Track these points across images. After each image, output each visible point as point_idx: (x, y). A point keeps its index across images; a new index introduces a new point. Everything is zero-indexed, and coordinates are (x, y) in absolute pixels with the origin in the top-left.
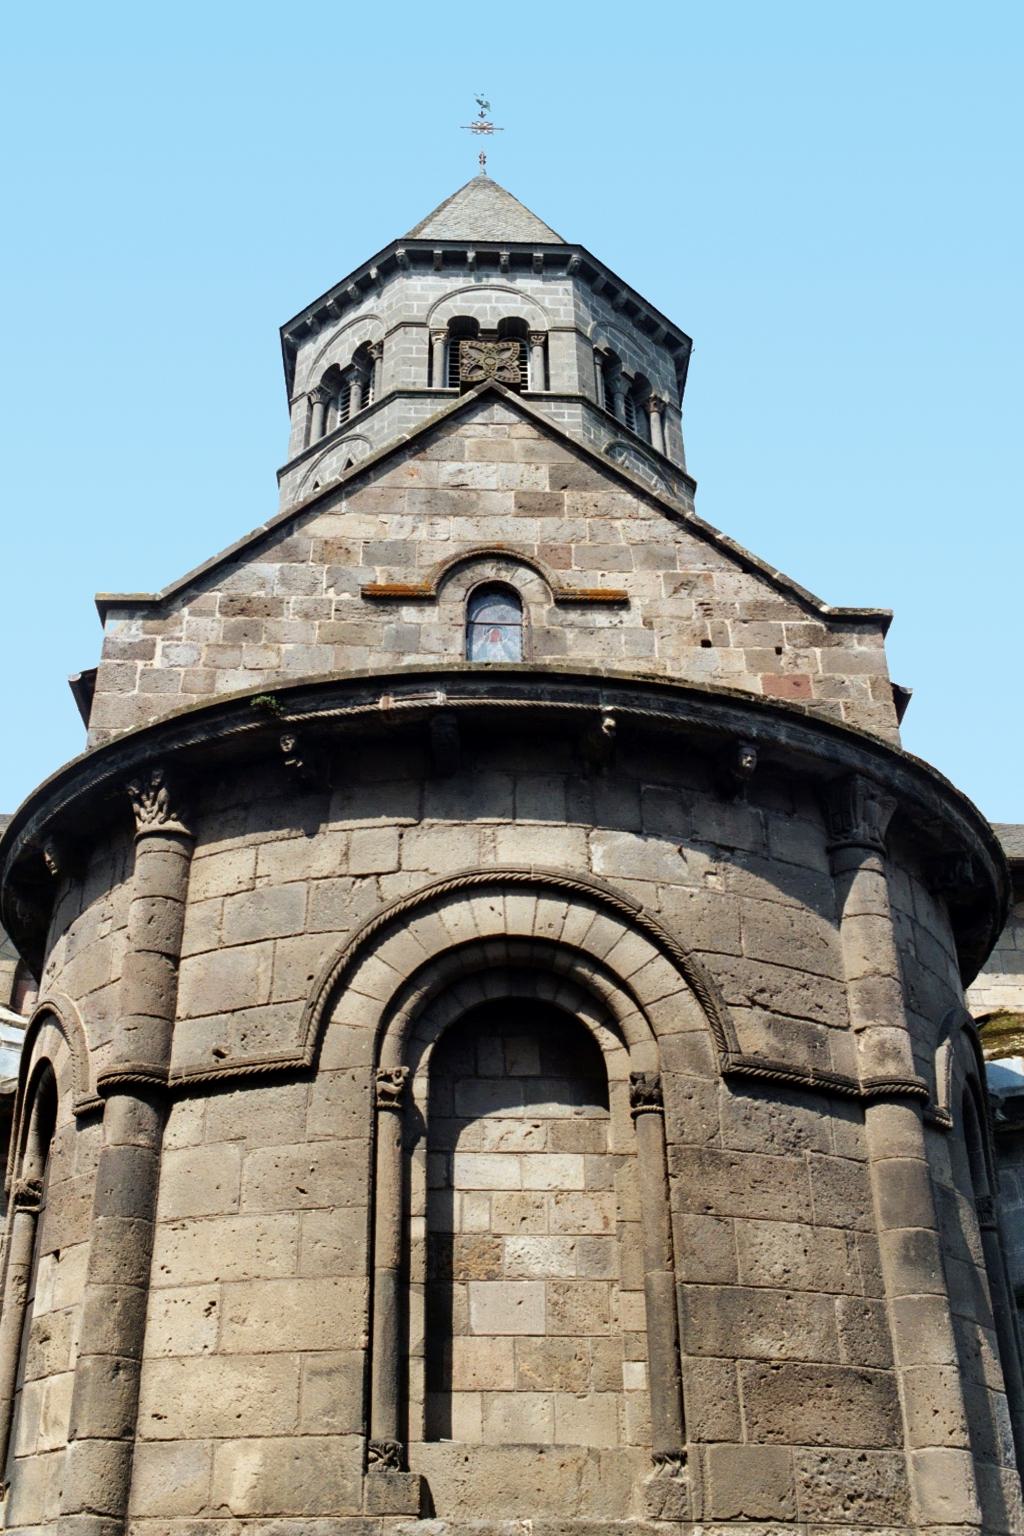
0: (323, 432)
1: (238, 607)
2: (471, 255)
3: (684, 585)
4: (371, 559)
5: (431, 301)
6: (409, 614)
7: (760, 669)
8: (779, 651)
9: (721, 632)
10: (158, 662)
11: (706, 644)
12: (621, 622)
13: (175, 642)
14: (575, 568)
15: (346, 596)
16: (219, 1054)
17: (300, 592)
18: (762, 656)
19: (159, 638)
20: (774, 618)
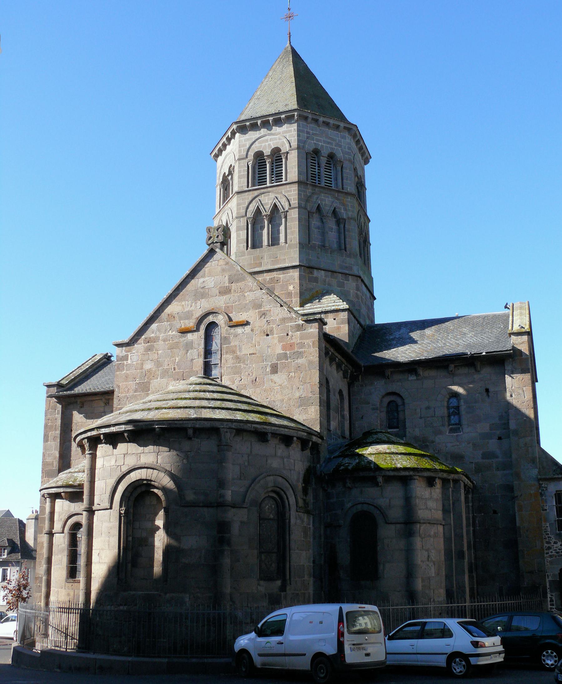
0: (232, 193)
1: (148, 341)
2: (259, 122)
3: (264, 314)
4: (181, 319)
5: (248, 146)
6: (189, 336)
7: (281, 342)
8: (288, 335)
9: (272, 331)
10: (129, 362)
11: (268, 335)
12: (245, 331)
13: (133, 354)
14: (234, 313)
15: (174, 333)
16: (522, 327)
17: (162, 333)
18: (283, 337)
19: (129, 353)
20: (287, 323)
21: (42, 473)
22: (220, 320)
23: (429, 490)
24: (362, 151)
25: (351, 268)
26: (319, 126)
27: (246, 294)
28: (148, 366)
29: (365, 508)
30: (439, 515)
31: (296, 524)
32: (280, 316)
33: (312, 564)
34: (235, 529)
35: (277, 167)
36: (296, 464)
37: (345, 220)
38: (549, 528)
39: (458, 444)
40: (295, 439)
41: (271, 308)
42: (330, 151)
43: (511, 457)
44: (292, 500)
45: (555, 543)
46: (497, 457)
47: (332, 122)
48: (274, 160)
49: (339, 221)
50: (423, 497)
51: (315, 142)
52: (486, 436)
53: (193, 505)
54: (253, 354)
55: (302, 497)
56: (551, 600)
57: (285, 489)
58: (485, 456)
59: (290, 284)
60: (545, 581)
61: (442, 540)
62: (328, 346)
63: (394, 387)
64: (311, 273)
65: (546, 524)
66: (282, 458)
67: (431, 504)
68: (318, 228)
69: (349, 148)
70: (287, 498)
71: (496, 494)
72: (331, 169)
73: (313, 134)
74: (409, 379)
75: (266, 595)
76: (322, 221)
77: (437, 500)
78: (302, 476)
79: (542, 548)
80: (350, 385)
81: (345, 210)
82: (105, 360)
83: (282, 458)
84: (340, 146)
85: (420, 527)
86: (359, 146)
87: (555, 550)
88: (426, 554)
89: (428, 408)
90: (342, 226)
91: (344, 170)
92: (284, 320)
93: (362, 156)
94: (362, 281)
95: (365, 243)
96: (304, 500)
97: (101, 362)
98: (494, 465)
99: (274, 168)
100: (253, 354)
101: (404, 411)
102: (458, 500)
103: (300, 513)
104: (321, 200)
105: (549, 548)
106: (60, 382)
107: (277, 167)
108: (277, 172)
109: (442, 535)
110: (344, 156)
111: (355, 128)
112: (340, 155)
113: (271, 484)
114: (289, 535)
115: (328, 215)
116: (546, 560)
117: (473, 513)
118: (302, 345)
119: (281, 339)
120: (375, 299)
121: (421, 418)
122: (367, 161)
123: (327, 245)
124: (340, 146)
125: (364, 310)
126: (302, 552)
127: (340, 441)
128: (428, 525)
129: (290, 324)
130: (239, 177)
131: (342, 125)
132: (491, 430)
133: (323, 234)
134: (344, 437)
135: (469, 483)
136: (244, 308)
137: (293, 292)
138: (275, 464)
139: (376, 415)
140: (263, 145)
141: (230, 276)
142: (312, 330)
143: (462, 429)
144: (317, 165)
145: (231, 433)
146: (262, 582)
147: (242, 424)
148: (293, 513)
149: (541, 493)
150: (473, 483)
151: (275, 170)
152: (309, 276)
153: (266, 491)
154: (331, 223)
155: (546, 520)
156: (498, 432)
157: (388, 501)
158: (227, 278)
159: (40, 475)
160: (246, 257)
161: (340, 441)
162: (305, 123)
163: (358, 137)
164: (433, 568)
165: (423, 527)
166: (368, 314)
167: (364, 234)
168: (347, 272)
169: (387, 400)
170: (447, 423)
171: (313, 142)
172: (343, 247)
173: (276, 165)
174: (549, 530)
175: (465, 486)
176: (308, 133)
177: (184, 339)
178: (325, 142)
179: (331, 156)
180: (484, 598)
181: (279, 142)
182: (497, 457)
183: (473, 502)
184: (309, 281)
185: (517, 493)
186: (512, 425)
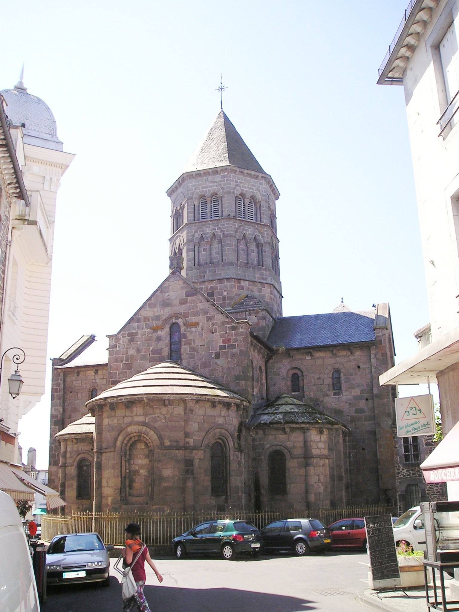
11: (213, 333)
19: (117, 343)
21: (51, 422)
22: (180, 321)
23: (319, 436)
24: (274, 192)
25: (266, 279)
26: (244, 176)
27: (197, 305)
28: (131, 352)
29: (278, 448)
30: (326, 452)
31: (233, 459)
32: (221, 320)
33: (243, 485)
34: (196, 463)
35: (214, 206)
36: (233, 420)
37: (262, 244)
38: (399, 460)
39: (339, 403)
40: (233, 404)
41: (215, 314)
42: (252, 195)
43: (374, 412)
44: (231, 444)
45: (403, 469)
46: (365, 412)
47: (253, 173)
48: (213, 201)
49: (259, 245)
50: (315, 441)
51: (241, 188)
52: (357, 398)
53: (170, 448)
54: (203, 345)
55: (237, 441)
56: (400, 508)
57: (226, 437)
58: (357, 411)
59: (225, 291)
60: (396, 495)
61: (328, 468)
62: (253, 339)
63: (296, 364)
64: (240, 283)
65: (397, 457)
66: (224, 417)
67: (321, 445)
68: (243, 250)
69: (265, 192)
70: (228, 443)
71: (365, 437)
72: (253, 206)
73: (240, 183)
74: (307, 358)
75: (215, 506)
76: (247, 245)
77: (324, 442)
78: (237, 428)
79: (394, 473)
80: (266, 362)
81: (263, 237)
82: (91, 339)
83: (224, 417)
84: (259, 190)
85: (313, 460)
86: (272, 189)
87: (403, 474)
88: (317, 478)
89: (319, 378)
90: (260, 248)
91: (261, 208)
92: (223, 323)
93: (274, 195)
94: (274, 287)
95: (276, 258)
96: (239, 444)
97: (88, 341)
98: (363, 417)
99: (213, 206)
100: (203, 345)
101: (303, 380)
102: (338, 442)
103: (236, 452)
104: (246, 230)
105: (399, 473)
106: (61, 357)
107: (214, 206)
108: (215, 210)
109: (327, 465)
110: (261, 198)
111: (269, 177)
112: (259, 197)
113: (218, 434)
114: (230, 468)
115: (250, 241)
116: (396, 481)
117: (349, 450)
118: (236, 340)
119: (221, 336)
120: (283, 297)
121: (314, 385)
122: (277, 198)
123: (250, 262)
124: (259, 190)
125: (275, 308)
126: (237, 477)
127: (260, 401)
128: (318, 459)
129: (227, 326)
130: (188, 213)
131: (260, 175)
132: (361, 393)
133: (248, 255)
134: (263, 399)
135: (346, 430)
136: (196, 314)
137: (227, 296)
138: (220, 421)
139: (284, 383)
140: (205, 190)
141: (186, 292)
142: (242, 330)
143: (342, 393)
144: (243, 205)
145: (193, 403)
146: (213, 497)
147: (200, 396)
148: (231, 451)
149: (394, 437)
150: (349, 430)
151: (213, 208)
152: (238, 285)
153: (215, 438)
154: (253, 247)
155: (397, 454)
156: (366, 395)
157: (292, 443)
158: (184, 293)
159: (50, 424)
160: (194, 271)
161: (260, 401)
162: (234, 175)
163: (272, 183)
164: (322, 487)
165: (315, 460)
166: (278, 309)
167: (275, 252)
168: (264, 281)
169: (291, 373)
170: (332, 389)
171: (240, 188)
172: (261, 264)
173: (214, 205)
174: (399, 461)
175: (343, 432)
176: (237, 182)
177: (155, 334)
178: (248, 188)
179: (253, 197)
180: (356, 506)
181: (215, 189)
182: (365, 412)
183: (349, 442)
184: (237, 289)
185: (378, 436)
186: (375, 391)
